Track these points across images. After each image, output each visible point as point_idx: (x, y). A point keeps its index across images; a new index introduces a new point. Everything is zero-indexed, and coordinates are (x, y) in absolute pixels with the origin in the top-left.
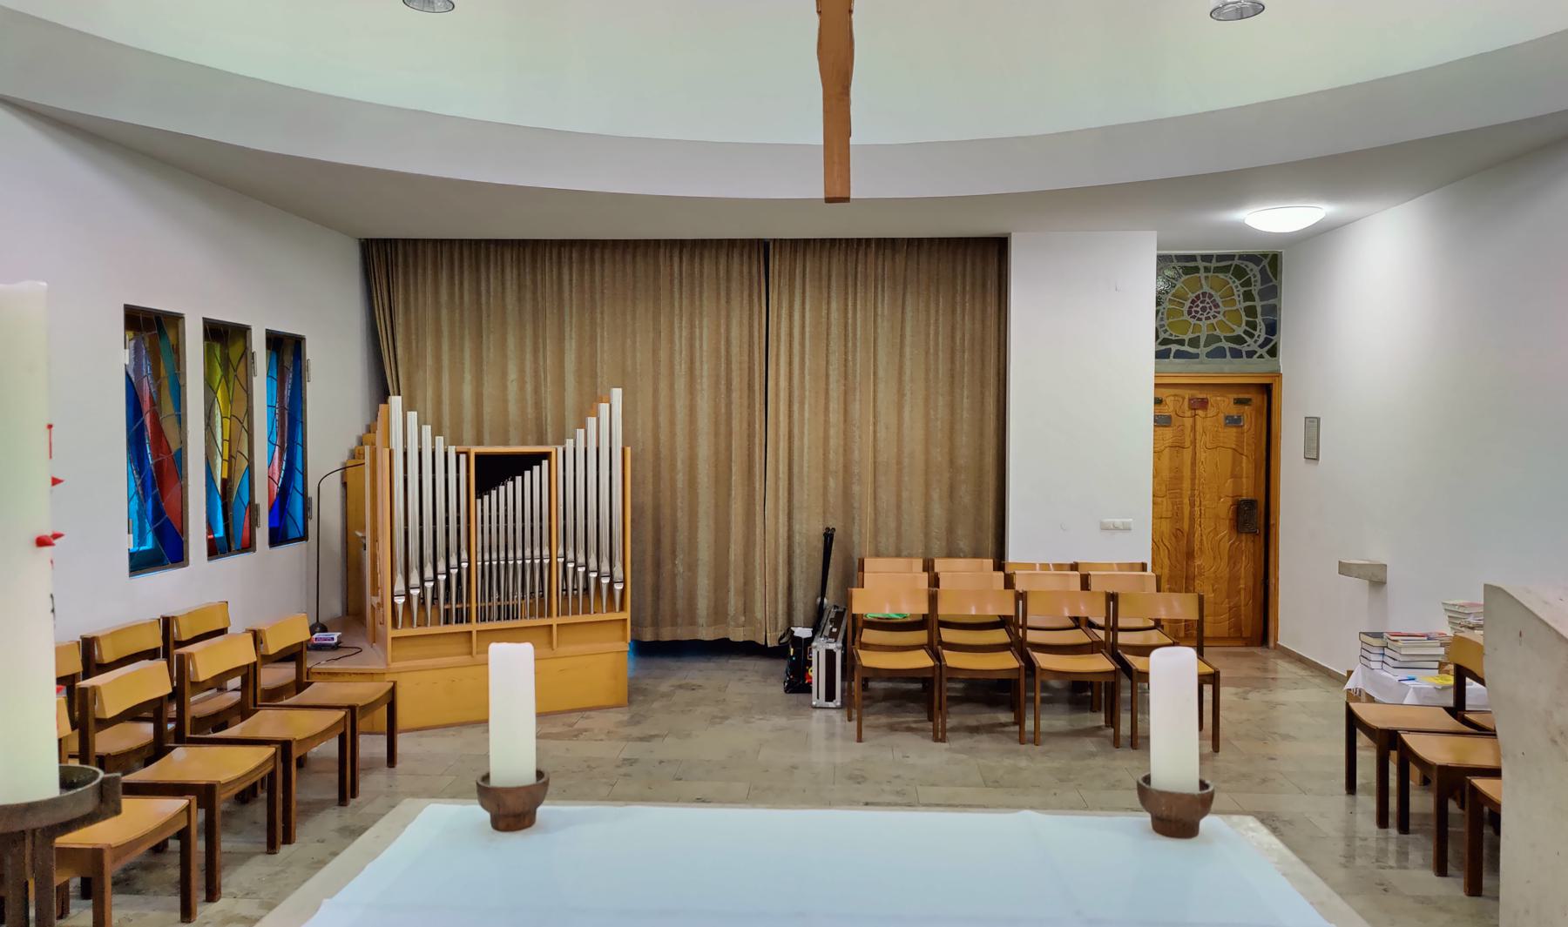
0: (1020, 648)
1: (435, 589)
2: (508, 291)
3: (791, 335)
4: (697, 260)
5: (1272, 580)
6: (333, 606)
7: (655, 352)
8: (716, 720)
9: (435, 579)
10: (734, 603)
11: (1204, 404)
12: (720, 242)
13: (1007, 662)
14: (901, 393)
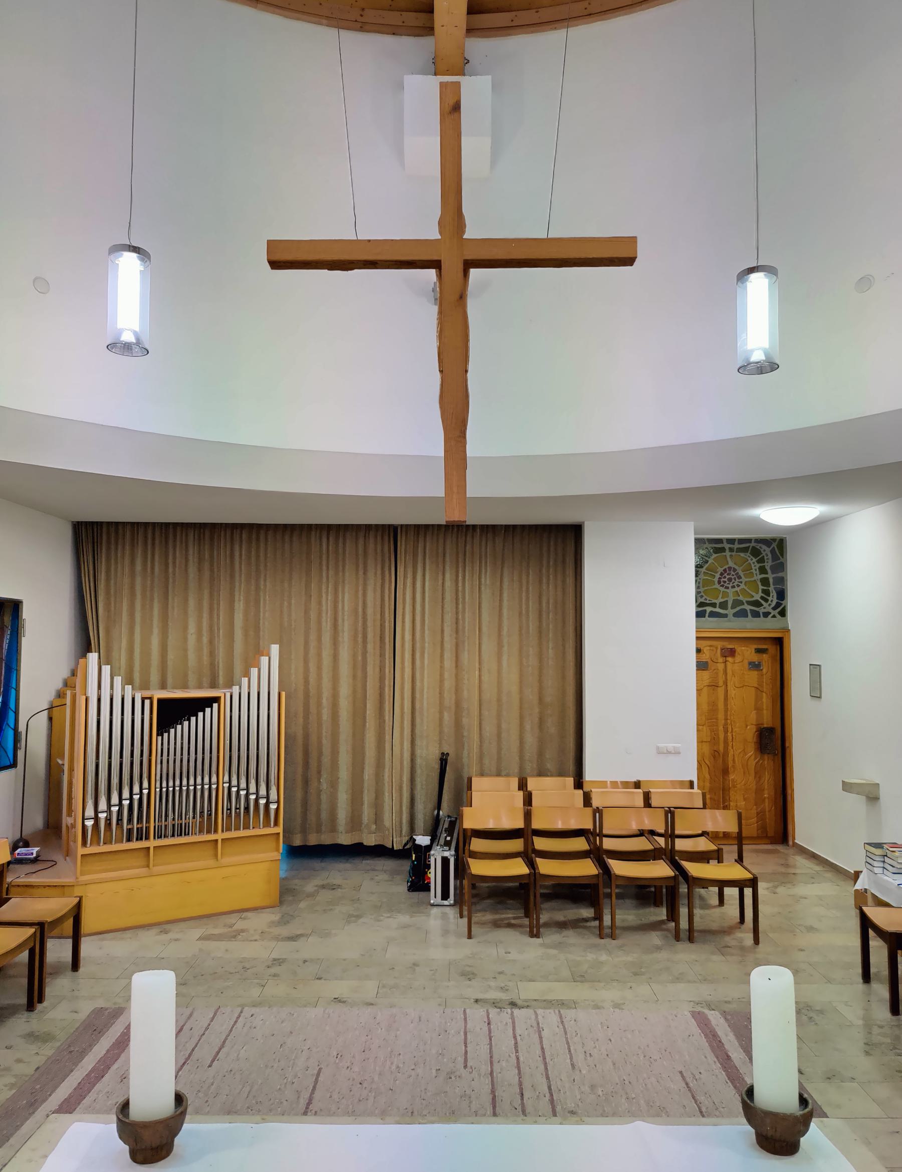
0: (597, 855)
1: (120, 812)
2: (191, 563)
4: (341, 540)
5: (789, 791)
6: (36, 821)
7: (307, 612)
8: (353, 918)
9: (120, 804)
10: (367, 814)
11: (732, 653)
13: (586, 868)
14: (500, 646)
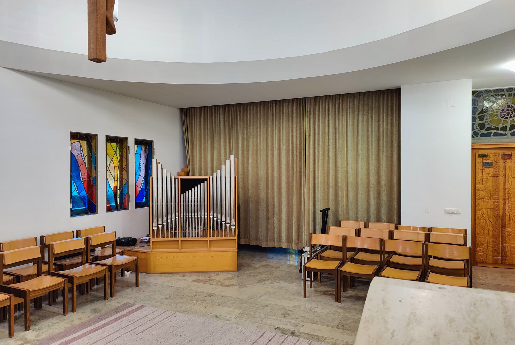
3: (314, 133)
11: (510, 157)
12: (289, 100)
